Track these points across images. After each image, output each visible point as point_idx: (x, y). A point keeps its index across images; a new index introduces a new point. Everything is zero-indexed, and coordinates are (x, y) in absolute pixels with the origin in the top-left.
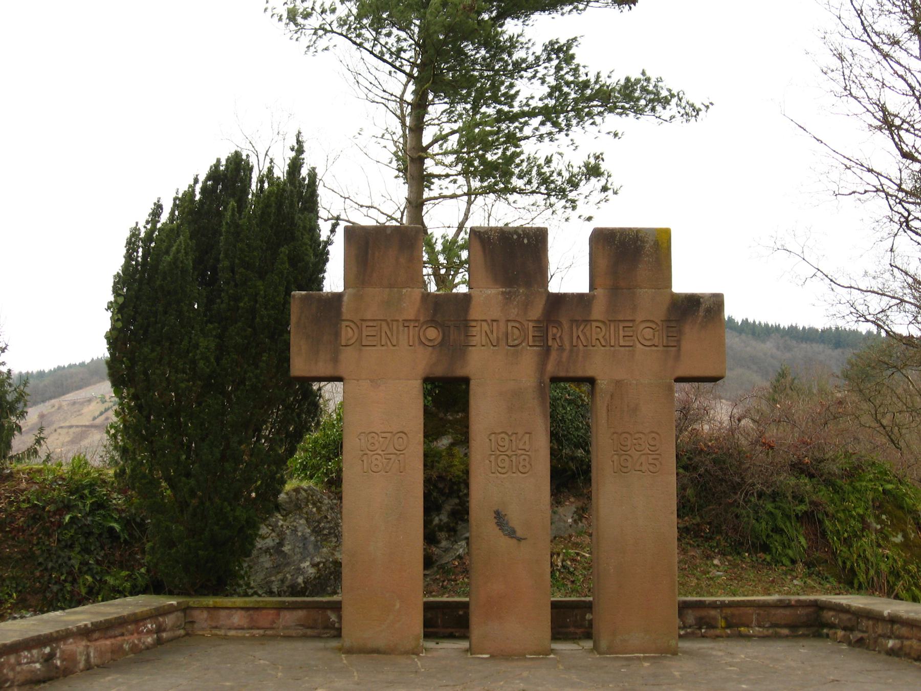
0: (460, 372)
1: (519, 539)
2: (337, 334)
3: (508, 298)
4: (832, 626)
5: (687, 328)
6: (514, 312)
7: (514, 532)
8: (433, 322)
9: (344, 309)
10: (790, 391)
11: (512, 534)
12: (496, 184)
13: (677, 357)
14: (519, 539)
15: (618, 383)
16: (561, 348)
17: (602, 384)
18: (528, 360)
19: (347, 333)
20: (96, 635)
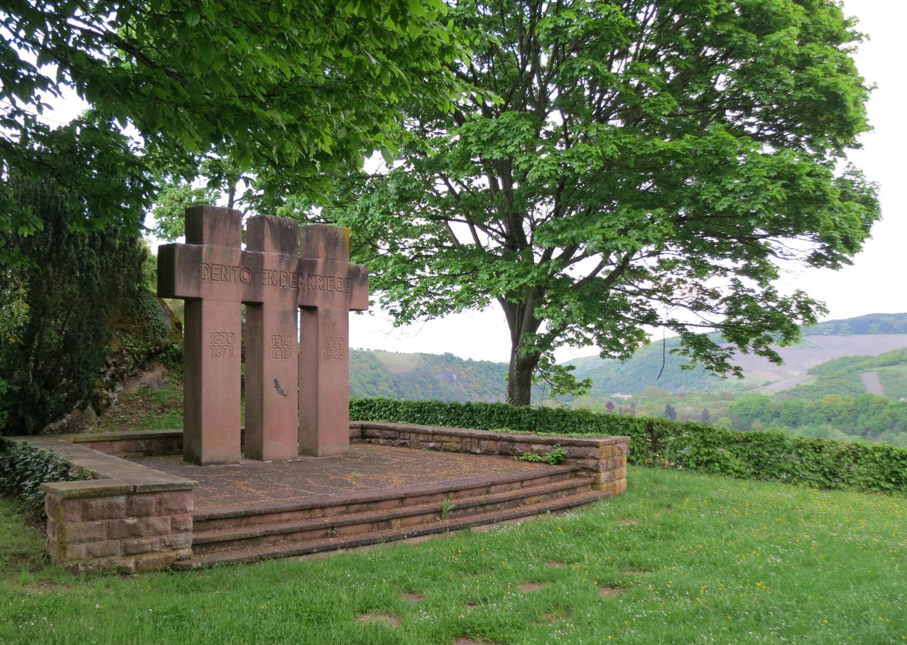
0: (259, 300)
1: (285, 396)
2: (199, 271)
3: (282, 258)
4: (378, 437)
5: (355, 283)
6: (284, 267)
7: (282, 391)
8: (248, 269)
9: (204, 256)
10: (681, 277)
11: (282, 393)
12: (612, 53)
13: (351, 299)
14: (285, 396)
15: (327, 311)
16: (303, 289)
17: (321, 310)
18: (290, 294)
19: (205, 272)
20: (488, 507)
